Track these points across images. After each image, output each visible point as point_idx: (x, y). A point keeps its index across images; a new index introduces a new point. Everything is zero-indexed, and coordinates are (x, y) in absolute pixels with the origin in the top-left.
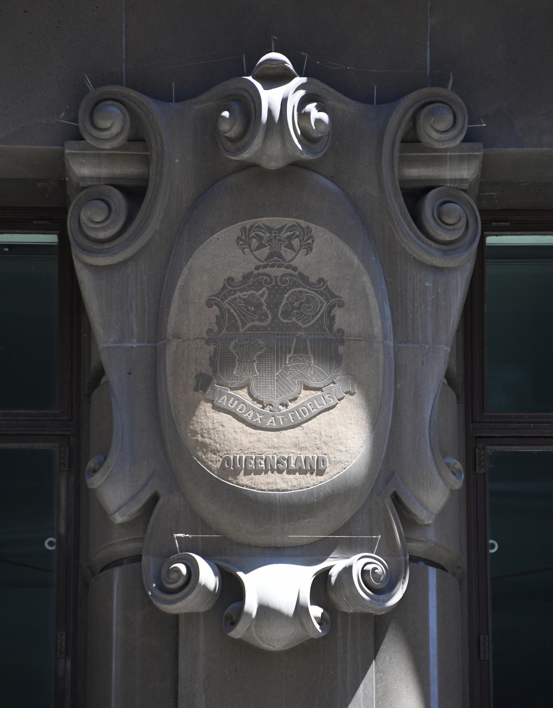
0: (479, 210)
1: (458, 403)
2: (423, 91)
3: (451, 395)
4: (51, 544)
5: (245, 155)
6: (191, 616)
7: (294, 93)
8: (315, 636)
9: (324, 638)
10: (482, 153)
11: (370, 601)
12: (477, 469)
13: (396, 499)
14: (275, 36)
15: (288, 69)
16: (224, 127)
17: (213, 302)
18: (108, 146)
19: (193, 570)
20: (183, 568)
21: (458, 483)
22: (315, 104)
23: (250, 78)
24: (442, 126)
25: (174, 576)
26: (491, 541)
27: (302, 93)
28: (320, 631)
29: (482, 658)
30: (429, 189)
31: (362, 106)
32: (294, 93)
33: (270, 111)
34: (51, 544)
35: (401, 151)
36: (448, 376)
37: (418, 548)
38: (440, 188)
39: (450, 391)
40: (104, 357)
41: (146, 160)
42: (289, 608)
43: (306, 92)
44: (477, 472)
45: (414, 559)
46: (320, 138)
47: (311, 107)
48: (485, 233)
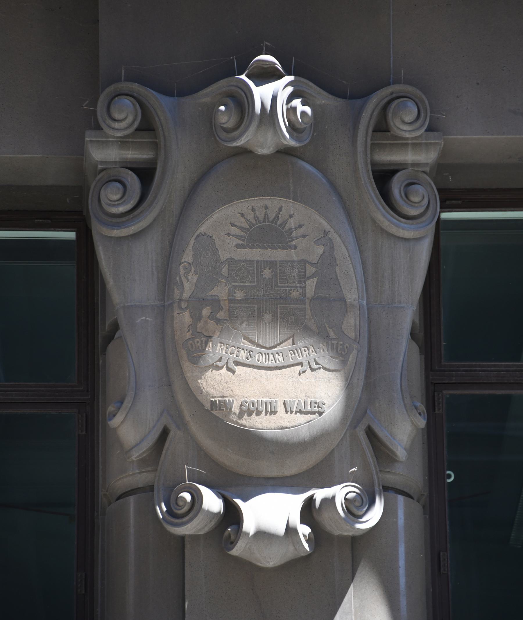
0: (438, 190)
1: (420, 355)
6: (195, 538)
7: (283, 89)
9: (308, 557)
12: (436, 409)
13: (371, 433)
14: (268, 42)
19: (197, 498)
20: (187, 496)
21: (422, 423)
22: (300, 100)
23: (243, 77)
24: (409, 118)
25: (181, 503)
26: (448, 472)
27: (290, 89)
28: (308, 550)
29: (442, 572)
30: (394, 172)
32: (283, 89)
38: (405, 170)
39: (414, 344)
41: (156, 146)
42: (281, 530)
43: (294, 88)
44: (436, 412)
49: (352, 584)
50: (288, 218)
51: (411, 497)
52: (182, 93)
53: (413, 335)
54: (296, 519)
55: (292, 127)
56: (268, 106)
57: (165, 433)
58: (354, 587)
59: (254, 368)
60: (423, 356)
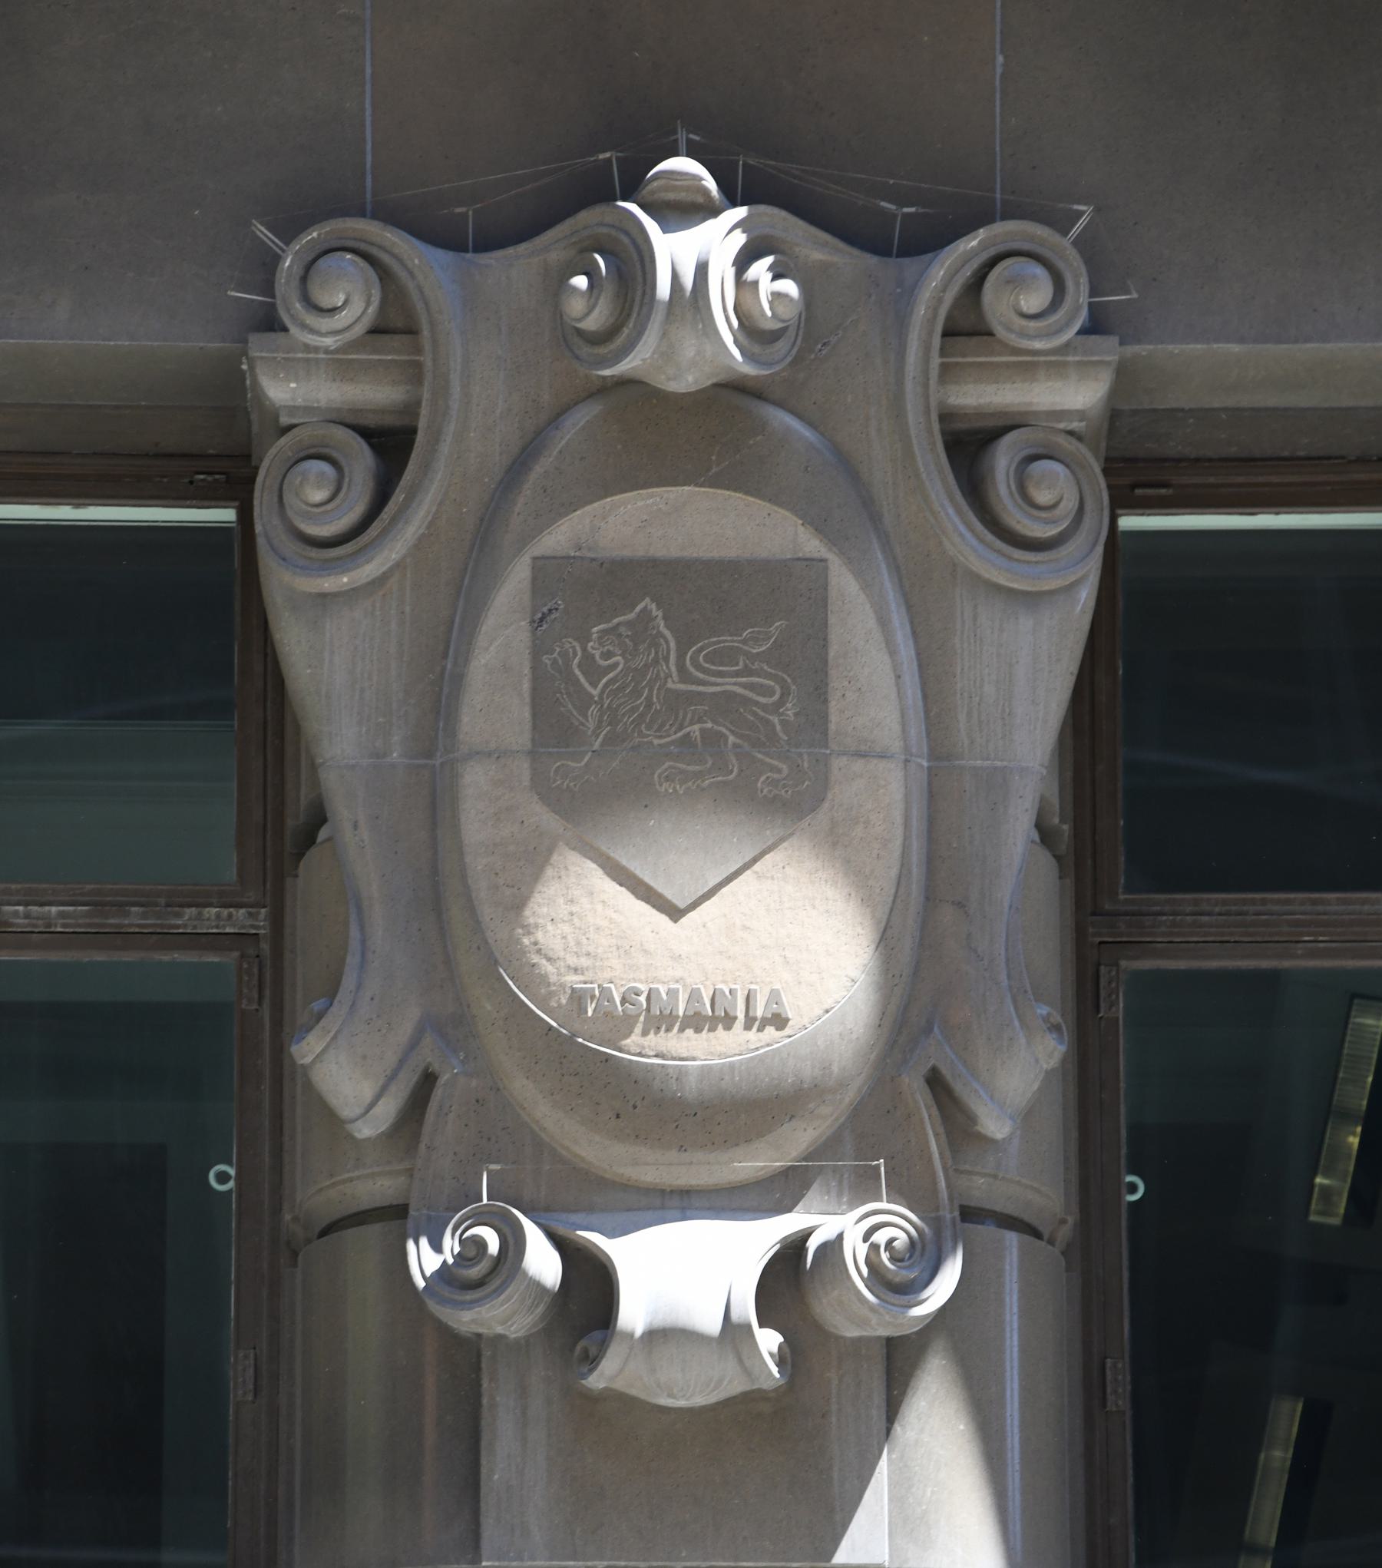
2: (1000, 228)
3: (1045, 861)
4: (223, 1178)
5: (625, 366)
7: (727, 235)
8: (767, 1385)
10: (1116, 358)
11: (879, 1305)
15: (706, 192)
16: (575, 307)
17: (680, 787)
18: (329, 341)
19: (514, 1244)
26: (1130, 1178)
27: (740, 239)
28: (778, 1376)
31: (872, 260)
32: (727, 235)
33: (675, 277)
34: (223, 1178)
35: (943, 352)
36: (1040, 826)
37: (980, 1190)
40: (332, 782)
41: (414, 373)
42: (712, 1324)
45: (969, 1214)
46: (784, 330)
47: (760, 269)
48: (1119, 512)
49: (883, 1464)
50: (568, 962)
51: (1036, 1234)
52: (487, 243)
53: (1045, 833)
54: (746, 1308)
55: (749, 329)
56: (688, 281)
57: (428, 1080)
58: (889, 1459)
59: (660, 896)
60: (1069, 882)
